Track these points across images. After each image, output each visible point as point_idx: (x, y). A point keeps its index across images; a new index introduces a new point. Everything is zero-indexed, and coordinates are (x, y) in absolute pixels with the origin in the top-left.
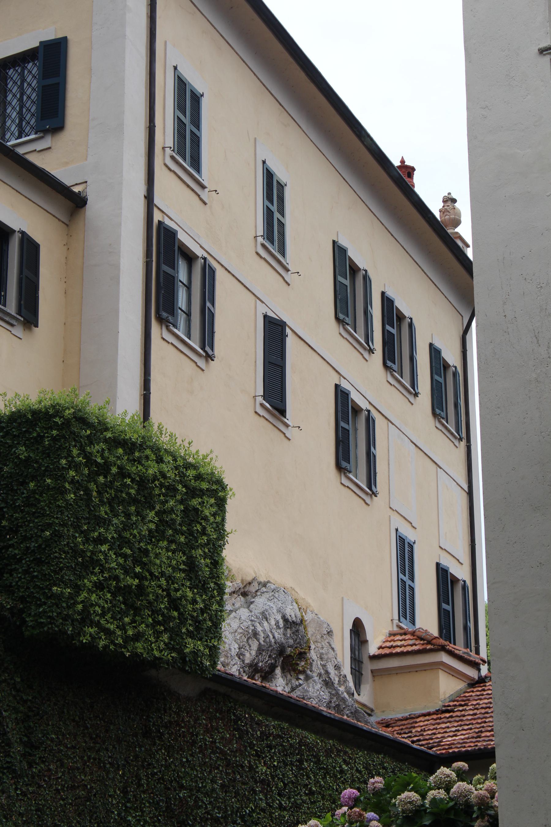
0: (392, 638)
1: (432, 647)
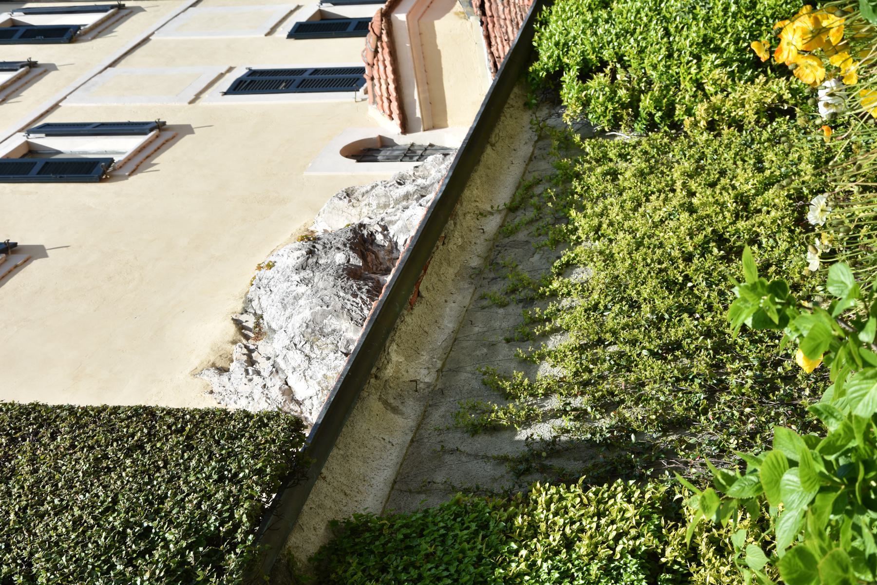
0: (378, 99)
1: (384, 32)
